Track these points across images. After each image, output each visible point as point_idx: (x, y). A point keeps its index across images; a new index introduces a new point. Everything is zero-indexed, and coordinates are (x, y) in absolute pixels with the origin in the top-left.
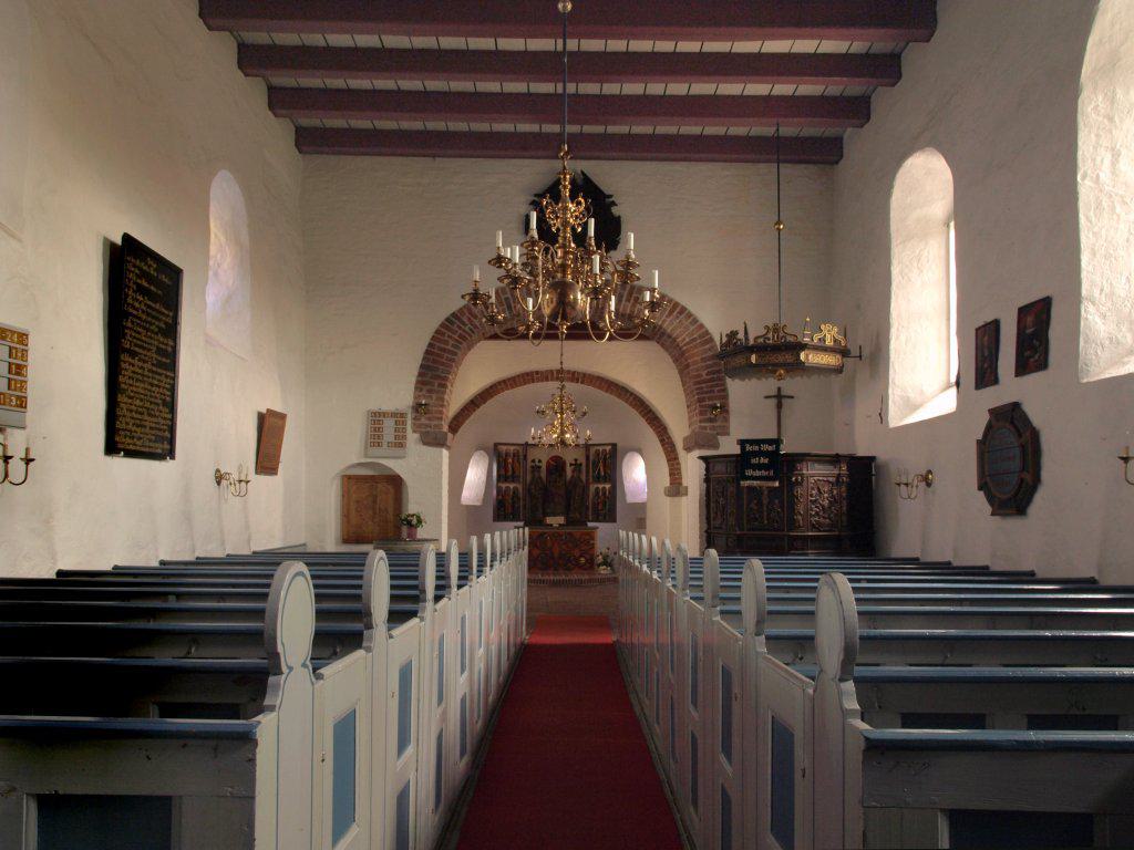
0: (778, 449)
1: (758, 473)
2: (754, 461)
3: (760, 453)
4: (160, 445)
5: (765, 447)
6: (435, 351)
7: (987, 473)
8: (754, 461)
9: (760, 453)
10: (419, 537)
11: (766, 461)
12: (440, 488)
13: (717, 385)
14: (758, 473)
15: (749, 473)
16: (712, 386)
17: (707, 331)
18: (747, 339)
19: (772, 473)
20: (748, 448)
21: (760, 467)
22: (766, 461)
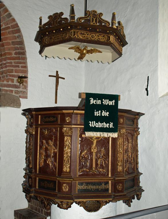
0: (116, 103)
1: (99, 125)
2: (97, 114)
3: (102, 107)
4: (56, 103)
5: (106, 102)
6: (11, 41)
7: (28, 124)
8: (97, 114)
9: (102, 107)
10: (68, 170)
11: (107, 114)
12: (40, 132)
13: (21, 63)
14: (99, 125)
15: (92, 124)
16: (18, 63)
17: (17, 24)
18: (73, 17)
19: (111, 125)
20: (92, 101)
21: (101, 119)
22: (107, 114)
